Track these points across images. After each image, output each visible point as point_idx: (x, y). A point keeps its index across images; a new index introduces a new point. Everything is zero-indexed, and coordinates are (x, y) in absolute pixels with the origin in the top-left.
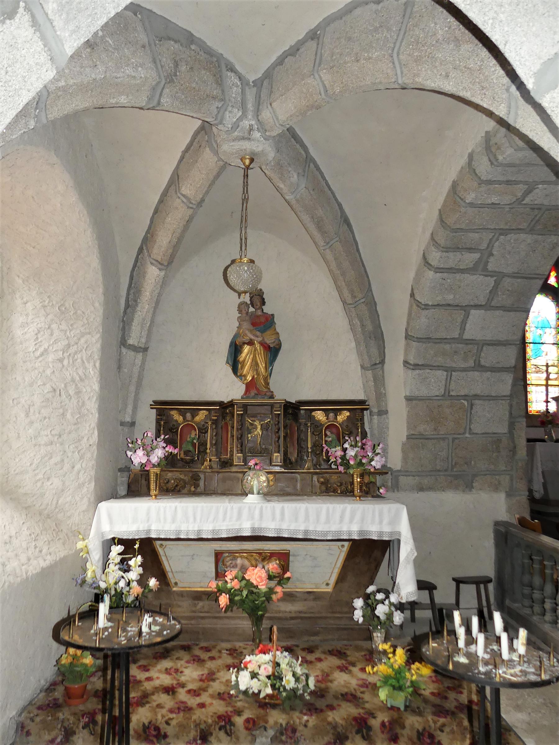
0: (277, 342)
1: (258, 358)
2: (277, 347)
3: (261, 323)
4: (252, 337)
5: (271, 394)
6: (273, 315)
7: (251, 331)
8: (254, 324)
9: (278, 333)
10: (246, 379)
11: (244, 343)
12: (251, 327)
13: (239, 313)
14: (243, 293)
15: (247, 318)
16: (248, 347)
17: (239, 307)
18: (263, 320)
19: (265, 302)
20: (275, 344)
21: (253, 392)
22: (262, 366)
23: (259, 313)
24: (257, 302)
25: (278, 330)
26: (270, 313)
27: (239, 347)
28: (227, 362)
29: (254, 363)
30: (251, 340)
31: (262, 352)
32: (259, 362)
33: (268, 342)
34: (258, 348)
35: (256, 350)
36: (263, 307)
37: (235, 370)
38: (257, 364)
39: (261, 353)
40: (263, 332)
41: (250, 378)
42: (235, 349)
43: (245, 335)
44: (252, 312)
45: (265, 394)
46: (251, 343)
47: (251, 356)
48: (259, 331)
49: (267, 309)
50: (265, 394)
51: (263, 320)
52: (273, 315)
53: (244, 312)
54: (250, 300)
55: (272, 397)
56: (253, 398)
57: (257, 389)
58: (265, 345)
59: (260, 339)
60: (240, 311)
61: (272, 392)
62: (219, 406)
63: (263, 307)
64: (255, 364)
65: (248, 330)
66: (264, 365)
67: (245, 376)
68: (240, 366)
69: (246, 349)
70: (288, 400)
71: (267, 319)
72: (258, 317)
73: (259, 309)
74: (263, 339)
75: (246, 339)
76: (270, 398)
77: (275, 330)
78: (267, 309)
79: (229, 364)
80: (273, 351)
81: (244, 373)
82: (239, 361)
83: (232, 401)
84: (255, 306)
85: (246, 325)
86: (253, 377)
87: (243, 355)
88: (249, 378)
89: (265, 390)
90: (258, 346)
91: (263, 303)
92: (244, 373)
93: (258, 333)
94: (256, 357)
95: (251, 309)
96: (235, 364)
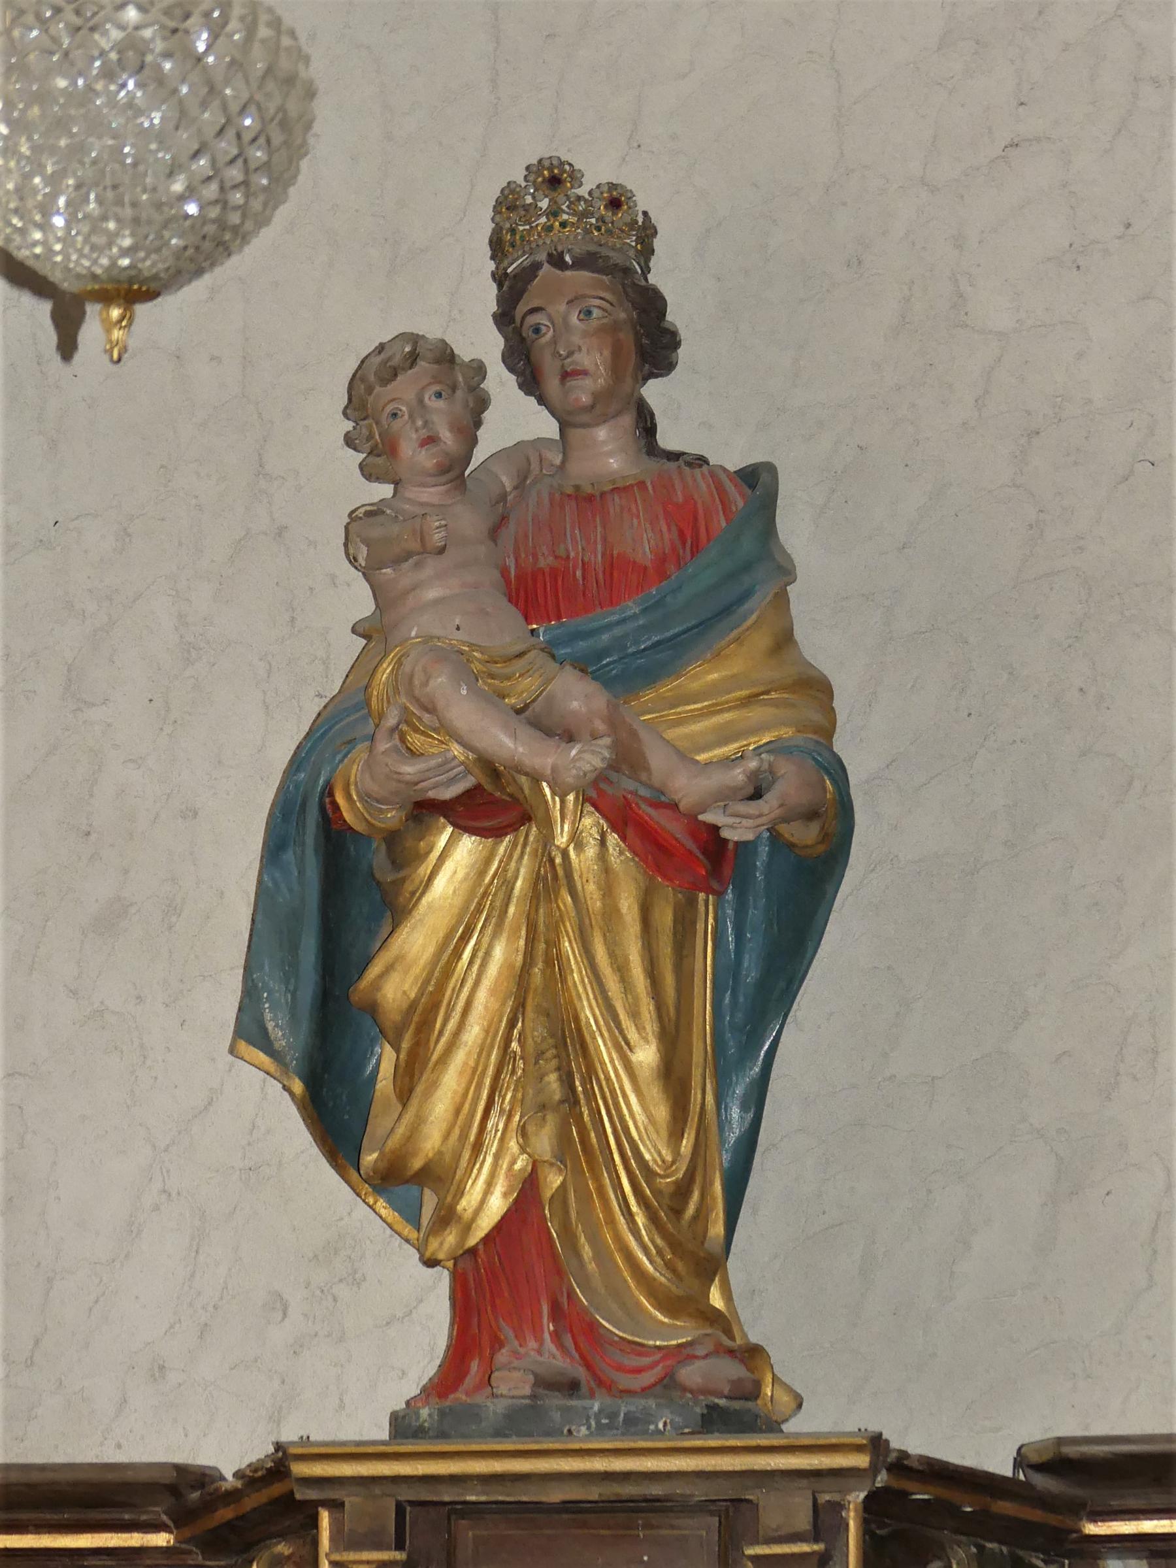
0: (790, 787)
1: (577, 975)
2: (804, 834)
3: (618, 577)
4: (508, 743)
5: (732, 1370)
6: (758, 481)
7: (486, 675)
8: (532, 593)
9: (816, 688)
10: (446, 1217)
11: (425, 811)
12: (506, 628)
13: (369, 473)
14: (106, 297)
15: (469, 521)
16: (467, 848)
17: (358, 403)
18: (642, 540)
19: (671, 340)
20: (769, 806)
21: (526, 1358)
22: (630, 1065)
23: (608, 453)
24: (584, 346)
25: (821, 642)
26: (731, 456)
27: (379, 859)
28: (250, 1030)
29: (534, 1028)
30: (489, 767)
31: (628, 905)
32: (590, 1014)
33: (687, 788)
34: (584, 861)
35: (552, 878)
36: (654, 392)
37: (335, 1112)
38: (568, 1044)
39: (611, 913)
40: (629, 672)
41: (497, 1205)
42: (332, 879)
43: (425, 714)
44: (522, 456)
45: (668, 1385)
46: (492, 805)
47: (502, 954)
48: (584, 665)
49: (693, 411)
50: (668, 1385)
51: (642, 540)
52: (758, 481)
53: (413, 454)
54: (504, 318)
55: (738, 1411)
56: (522, 1421)
57: (578, 1328)
58: (673, 828)
59: (586, 759)
60: (377, 452)
61: (753, 1354)
62: (180, 1519)
63: (654, 392)
64: (551, 1048)
65: (459, 661)
66: (646, 1055)
67: (441, 1177)
68: (386, 1060)
69: (454, 862)
70: (917, 1440)
71: (690, 534)
72: (589, 502)
73: (601, 408)
74: (627, 757)
75: (443, 769)
76: (715, 1419)
77: (785, 640)
78: (693, 411)
79: (264, 1042)
80: (759, 888)
81: (432, 1141)
82: (372, 1009)
83: (277, 1466)
84: (552, 385)
85: (454, 605)
86: (527, 1192)
87: (416, 942)
88: (486, 1201)
89: (668, 1331)
90: (582, 839)
91: (651, 341)
92: (432, 1141)
93: (577, 696)
94: (555, 963)
95: (515, 419)
96: (332, 1048)
